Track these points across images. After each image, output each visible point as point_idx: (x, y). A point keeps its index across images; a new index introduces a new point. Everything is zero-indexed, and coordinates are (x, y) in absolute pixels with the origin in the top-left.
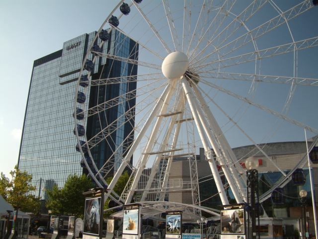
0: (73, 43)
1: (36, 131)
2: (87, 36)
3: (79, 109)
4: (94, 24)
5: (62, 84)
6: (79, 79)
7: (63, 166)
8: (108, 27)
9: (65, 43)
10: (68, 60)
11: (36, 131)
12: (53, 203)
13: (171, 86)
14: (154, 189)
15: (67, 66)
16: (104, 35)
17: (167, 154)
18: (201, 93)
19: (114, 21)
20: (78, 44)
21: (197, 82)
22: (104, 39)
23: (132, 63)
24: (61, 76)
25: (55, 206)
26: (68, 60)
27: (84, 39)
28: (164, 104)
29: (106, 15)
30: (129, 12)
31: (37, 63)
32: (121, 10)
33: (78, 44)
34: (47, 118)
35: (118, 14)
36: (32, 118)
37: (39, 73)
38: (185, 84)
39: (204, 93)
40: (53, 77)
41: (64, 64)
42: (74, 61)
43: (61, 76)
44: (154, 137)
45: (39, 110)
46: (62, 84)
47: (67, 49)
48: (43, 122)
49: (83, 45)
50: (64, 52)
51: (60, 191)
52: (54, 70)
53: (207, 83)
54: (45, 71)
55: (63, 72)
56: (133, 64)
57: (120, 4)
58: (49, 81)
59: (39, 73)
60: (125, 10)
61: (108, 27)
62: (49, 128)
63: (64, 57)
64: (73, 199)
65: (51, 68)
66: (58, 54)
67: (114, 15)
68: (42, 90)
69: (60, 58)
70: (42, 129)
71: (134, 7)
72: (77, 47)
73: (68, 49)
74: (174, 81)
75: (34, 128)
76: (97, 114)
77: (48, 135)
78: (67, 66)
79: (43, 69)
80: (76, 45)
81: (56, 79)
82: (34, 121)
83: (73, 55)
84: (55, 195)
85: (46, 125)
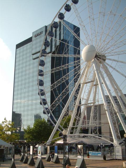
0: (38, 32)
1: (21, 89)
2: (46, 27)
3: (41, 70)
4: (48, 19)
5: (34, 59)
6: (41, 52)
7: (33, 112)
8: (57, 20)
9: (33, 33)
10: (36, 44)
11: (21, 89)
12: (28, 136)
13: (87, 66)
14: (85, 125)
15: (36, 48)
16: (55, 25)
17: (89, 105)
18: (107, 67)
19: (61, 16)
20: (41, 33)
21: (104, 60)
22: (56, 27)
23: (66, 56)
24: (33, 54)
25: (29, 137)
26: (36, 44)
27: (44, 30)
28: (84, 76)
29: (55, 12)
30: (70, 10)
31: (18, 46)
32: (65, 9)
33: (41, 33)
34: (27, 81)
35: (63, 11)
36: (18, 82)
37: (20, 53)
38: (95, 64)
39: (111, 67)
40: (28, 55)
41: (34, 47)
42: (38, 45)
43: (33, 54)
44: (92, 91)
45: (22, 76)
46: (34, 59)
47: (35, 37)
48: (25, 84)
49: (44, 33)
50: (33, 39)
51: (31, 129)
52: (28, 51)
53: (110, 59)
54: (23, 51)
55: (34, 52)
56: (66, 57)
57: (64, 5)
58: (26, 58)
59: (20, 53)
60: (68, 8)
61: (57, 20)
62: (29, 87)
63: (34, 42)
64: (41, 132)
65: (27, 49)
66: (29, 40)
67: (61, 12)
68: (23, 63)
69: (32, 42)
70: (25, 88)
71: (73, 6)
72: (40, 35)
73: (36, 36)
74: (89, 62)
75: (20, 87)
76: (53, 73)
77: (28, 92)
78: (36, 48)
79: (22, 50)
80: (40, 33)
81: (30, 56)
82: (20, 83)
83: (38, 40)
84: (28, 132)
85: (27, 85)
